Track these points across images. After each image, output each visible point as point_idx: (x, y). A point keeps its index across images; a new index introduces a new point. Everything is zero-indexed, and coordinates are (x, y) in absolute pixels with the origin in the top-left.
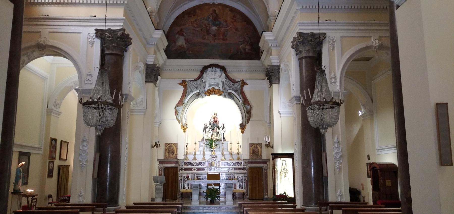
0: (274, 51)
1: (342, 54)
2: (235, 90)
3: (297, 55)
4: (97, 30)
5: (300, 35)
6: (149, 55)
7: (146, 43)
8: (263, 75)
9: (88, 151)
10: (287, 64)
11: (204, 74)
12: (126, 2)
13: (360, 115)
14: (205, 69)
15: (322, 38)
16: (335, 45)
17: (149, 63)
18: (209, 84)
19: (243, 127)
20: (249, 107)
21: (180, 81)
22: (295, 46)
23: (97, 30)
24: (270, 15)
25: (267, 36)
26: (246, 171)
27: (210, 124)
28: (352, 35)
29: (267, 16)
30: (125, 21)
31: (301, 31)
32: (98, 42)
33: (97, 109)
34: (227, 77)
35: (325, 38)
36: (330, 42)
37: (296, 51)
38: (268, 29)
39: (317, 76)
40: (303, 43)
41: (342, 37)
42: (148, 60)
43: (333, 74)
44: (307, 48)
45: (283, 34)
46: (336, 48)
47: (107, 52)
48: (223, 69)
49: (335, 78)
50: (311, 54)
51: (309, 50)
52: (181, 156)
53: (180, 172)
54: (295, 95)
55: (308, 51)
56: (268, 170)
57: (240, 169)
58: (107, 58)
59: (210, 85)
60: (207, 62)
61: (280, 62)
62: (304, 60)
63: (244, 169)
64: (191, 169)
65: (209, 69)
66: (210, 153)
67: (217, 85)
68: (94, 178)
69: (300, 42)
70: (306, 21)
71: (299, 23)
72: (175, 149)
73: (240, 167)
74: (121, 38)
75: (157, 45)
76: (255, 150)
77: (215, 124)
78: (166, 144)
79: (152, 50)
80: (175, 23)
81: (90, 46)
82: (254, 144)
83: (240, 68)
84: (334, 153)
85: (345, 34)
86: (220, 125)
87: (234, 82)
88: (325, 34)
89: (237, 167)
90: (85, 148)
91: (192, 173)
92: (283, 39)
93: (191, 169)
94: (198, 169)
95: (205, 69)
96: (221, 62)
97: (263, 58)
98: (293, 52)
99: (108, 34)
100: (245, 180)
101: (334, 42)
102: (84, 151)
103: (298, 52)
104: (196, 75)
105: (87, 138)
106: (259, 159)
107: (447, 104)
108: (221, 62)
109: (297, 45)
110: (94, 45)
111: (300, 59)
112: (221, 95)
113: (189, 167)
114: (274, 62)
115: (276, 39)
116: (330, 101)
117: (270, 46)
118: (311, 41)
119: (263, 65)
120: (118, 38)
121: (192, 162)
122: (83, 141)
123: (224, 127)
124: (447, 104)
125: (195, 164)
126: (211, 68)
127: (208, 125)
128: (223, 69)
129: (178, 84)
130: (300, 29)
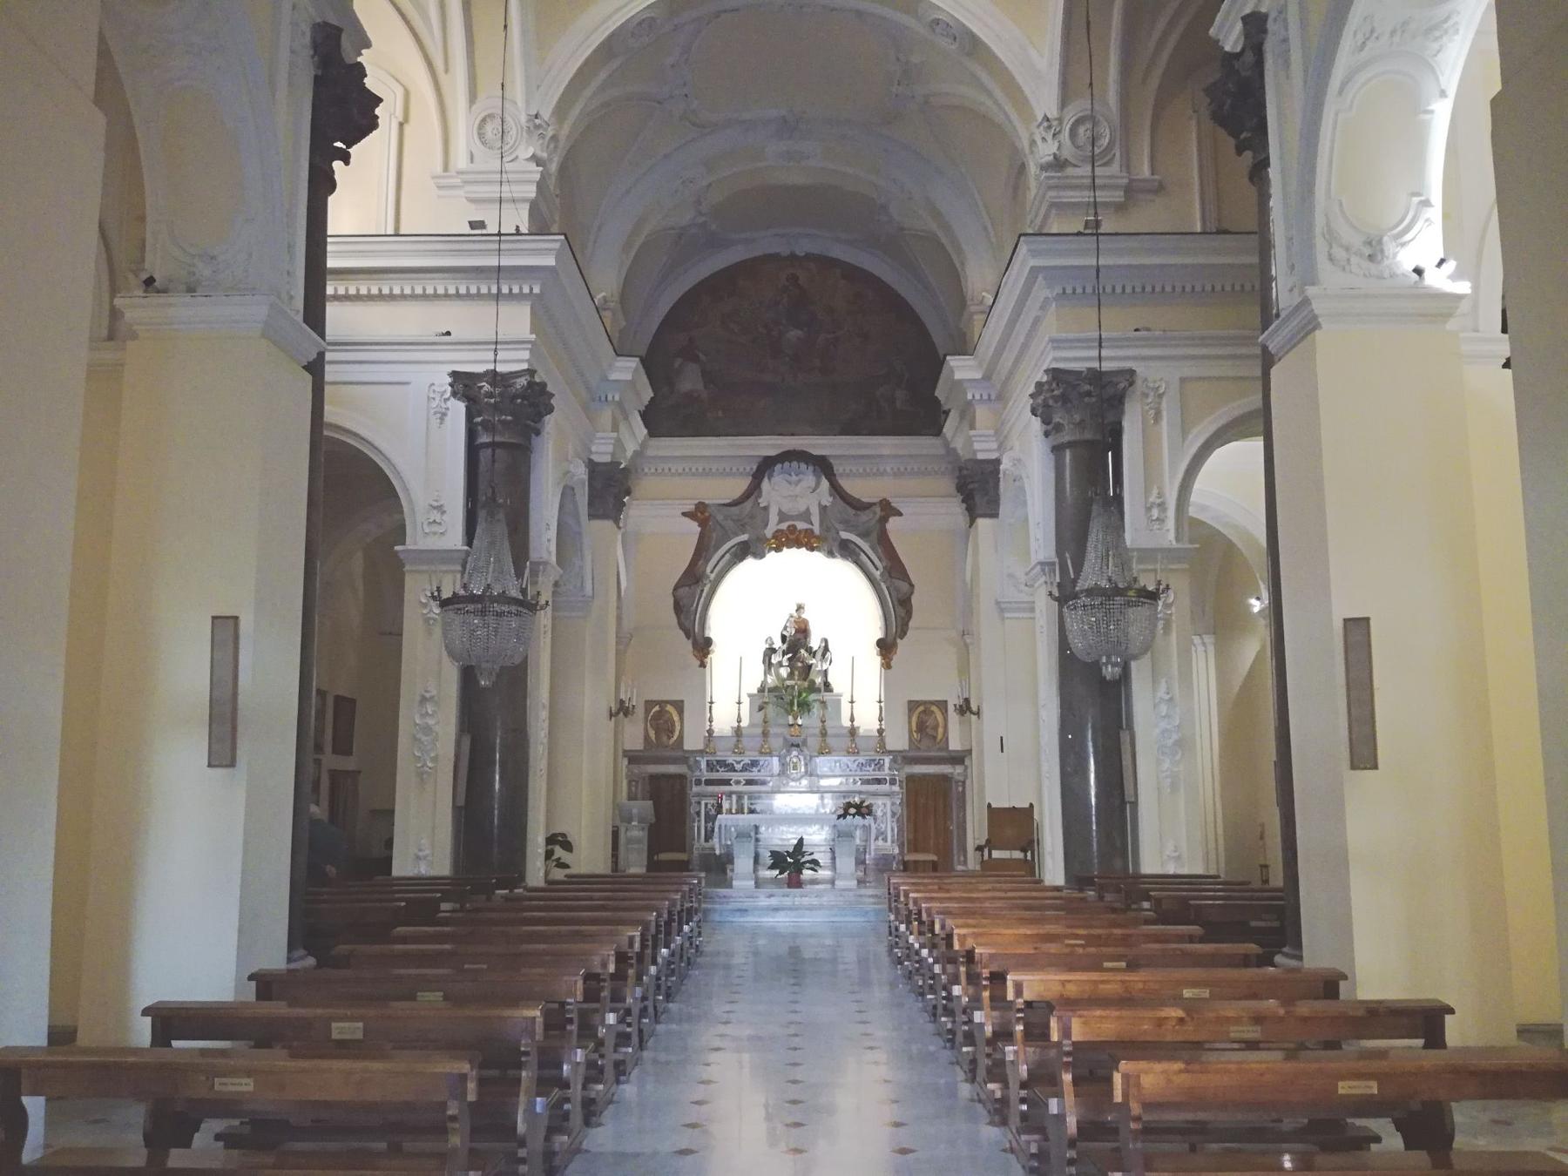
0: (981, 413)
1: (1185, 432)
2: (857, 531)
3: (1047, 434)
4: (455, 375)
5: (1054, 378)
6: (599, 435)
7: (593, 400)
8: (947, 484)
9: (437, 728)
10: (1019, 460)
11: (765, 485)
12: (536, 290)
13: (1256, 610)
14: (765, 467)
15: (1122, 385)
16: (1164, 405)
17: (596, 458)
18: (780, 513)
19: (886, 647)
20: (904, 586)
21: (690, 507)
22: (1042, 411)
23: (455, 375)
24: (969, 297)
25: (961, 368)
26: (896, 788)
27: (784, 638)
28: (1215, 372)
29: (962, 303)
30: (534, 348)
31: (1061, 365)
32: (459, 408)
33: (483, 613)
34: (836, 489)
35: (1131, 384)
36: (1146, 395)
37: (1046, 422)
38: (964, 347)
39: (1094, 514)
40: (1064, 399)
41: (1183, 380)
42: (594, 449)
43: (1155, 491)
44: (1077, 417)
45: (1022, 339)
46: (1164, 413)
47: (484, 438)
48: (823, 466)
49: (1162, 506)
50: (1088, 436)
51: (1082, 421)
52: (692, 742)
53: (695, 789)
54: (1041, 557)
55: (1081, 425)
56: (968, 782)
57: (879, 781)
58: (485, 455)
59: (783, 517)
60: (769, 445)
61: (1001, 447)
62: (1068, 454)
63: (893, 782)
64: (727, 782)
65: (778, 466)
66: (785, 731)
67: (806, 516)
68: (455, 808)
69: (1056, 399)
70: (1071, 336)
71: (1052, 341)
72: (676, 718)
73: (879, 775)
74: (524, 398)
75: (620, 404)
76: (924, 718)
77: (797, 639)
78: (649, 704)
79: (606, 416)
80: (669, 323)
81: (435, 421)
82: (924, 703)
83: (876, 463)
84: (1157, 731)
85: (1189, 370)
86: (815, 643)
87: (858, 506)
88: (1132, 372)
89: (871, 773)
90: (431, 722)
91: (730, 795)
92: (1008, 379)
93: (727, 782)
94: (749, 782)
95: (765, 467)
96: (818, 445)
97: (948, 429)
98: (1036, 424)
99: (487, 387)
100: (894, 814)
101: (1161, 396)
102: (427, 730)
103: (1051, 428)
104: (739, 486)
105: (434, 693)
106: (940, 750)
107: (1367, 620)
108: (818, 445)
109: (1046, 405)
110: (447, 419)
111: (1057, 450)
112: (818, 549)
113: (722, 774)
114: (984, 449)
115: (987, 377)
116: (1129, 588)
117: (970, 397)
118: (1089, 394)
119: (951, 452)
120: (515, 397)
121: (730, 760)
122: (424, 700)
123: (826, 649)
124: (1367, 620)
125: (738, 767)
126: (787, 464)
127: (778, 644)
128: (823, 466)
129: (684, 514)
130: (1055, 359)
